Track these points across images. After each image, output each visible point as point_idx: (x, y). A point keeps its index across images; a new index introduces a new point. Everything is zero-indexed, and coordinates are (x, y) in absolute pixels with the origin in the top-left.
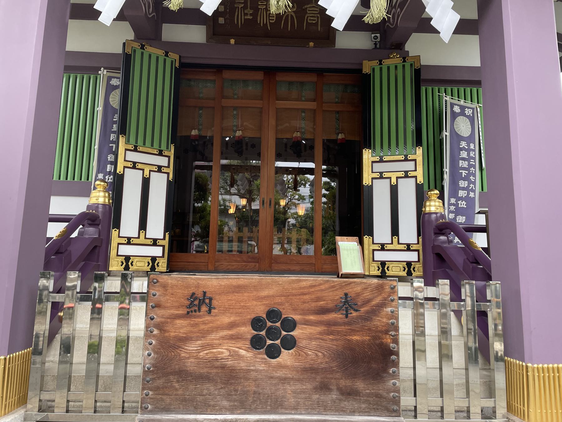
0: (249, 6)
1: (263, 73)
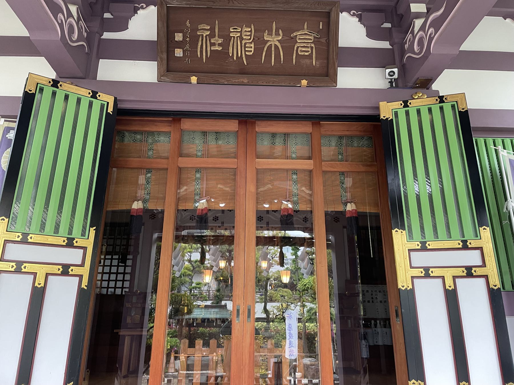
0: (217, 35)
1: (237, 121)
